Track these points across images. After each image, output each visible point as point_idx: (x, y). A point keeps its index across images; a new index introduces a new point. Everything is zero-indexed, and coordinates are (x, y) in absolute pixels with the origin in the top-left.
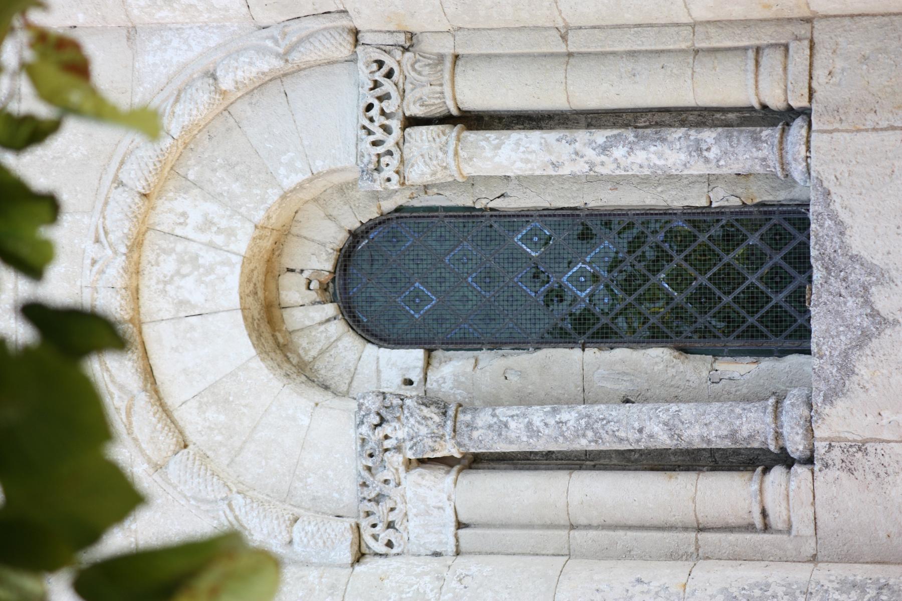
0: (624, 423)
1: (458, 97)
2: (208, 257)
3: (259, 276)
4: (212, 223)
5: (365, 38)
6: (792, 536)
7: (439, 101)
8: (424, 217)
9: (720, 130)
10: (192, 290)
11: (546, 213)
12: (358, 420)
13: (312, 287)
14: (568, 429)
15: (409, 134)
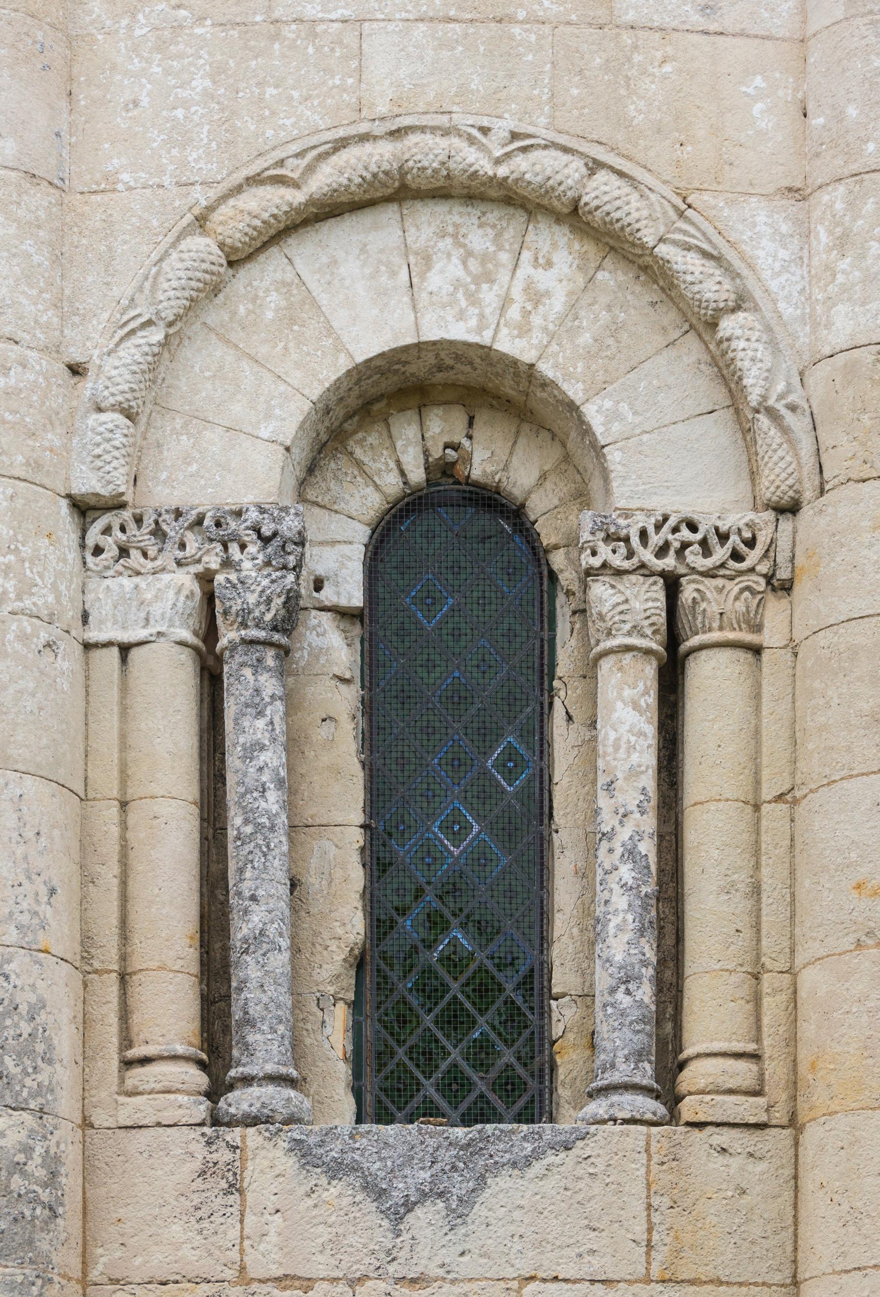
0: (263, 876)
1: (704, 654)
2: (490, 296)
3: (463, 374)
4: (537, 304)
5: (786, 524)
6: (116, 1096)
7: (700, 626)
8: (542, 609)
9: (653, 1008)
10: (445, 273)
11: (546, 778)
12: (267, 506)
13: (448, 451)
14: (255, 799)
15: (655, 583)
